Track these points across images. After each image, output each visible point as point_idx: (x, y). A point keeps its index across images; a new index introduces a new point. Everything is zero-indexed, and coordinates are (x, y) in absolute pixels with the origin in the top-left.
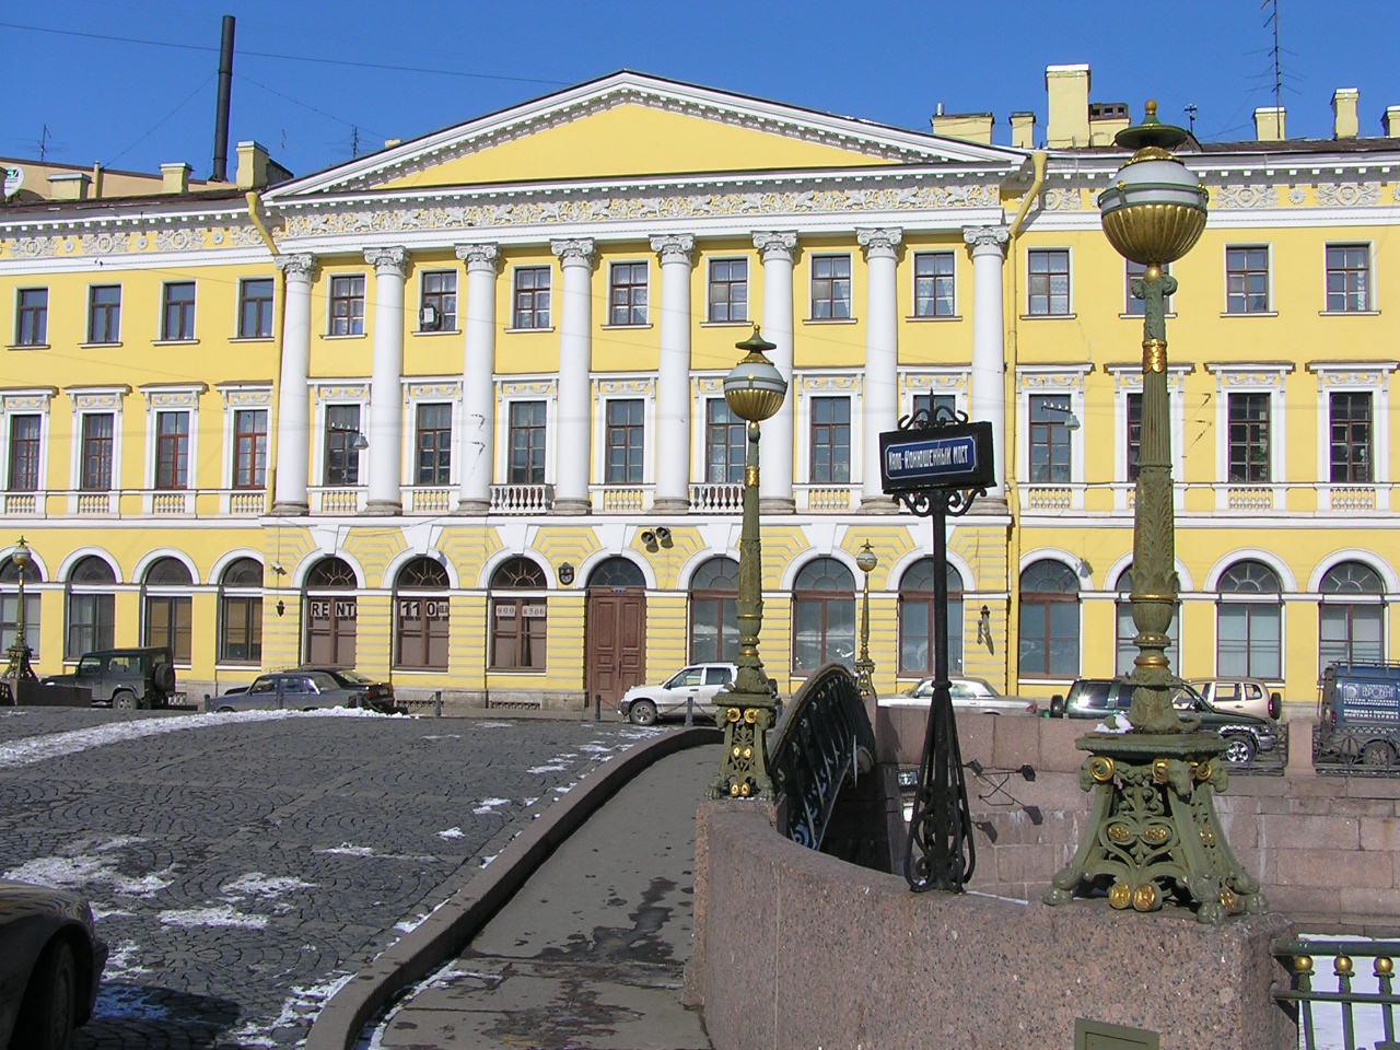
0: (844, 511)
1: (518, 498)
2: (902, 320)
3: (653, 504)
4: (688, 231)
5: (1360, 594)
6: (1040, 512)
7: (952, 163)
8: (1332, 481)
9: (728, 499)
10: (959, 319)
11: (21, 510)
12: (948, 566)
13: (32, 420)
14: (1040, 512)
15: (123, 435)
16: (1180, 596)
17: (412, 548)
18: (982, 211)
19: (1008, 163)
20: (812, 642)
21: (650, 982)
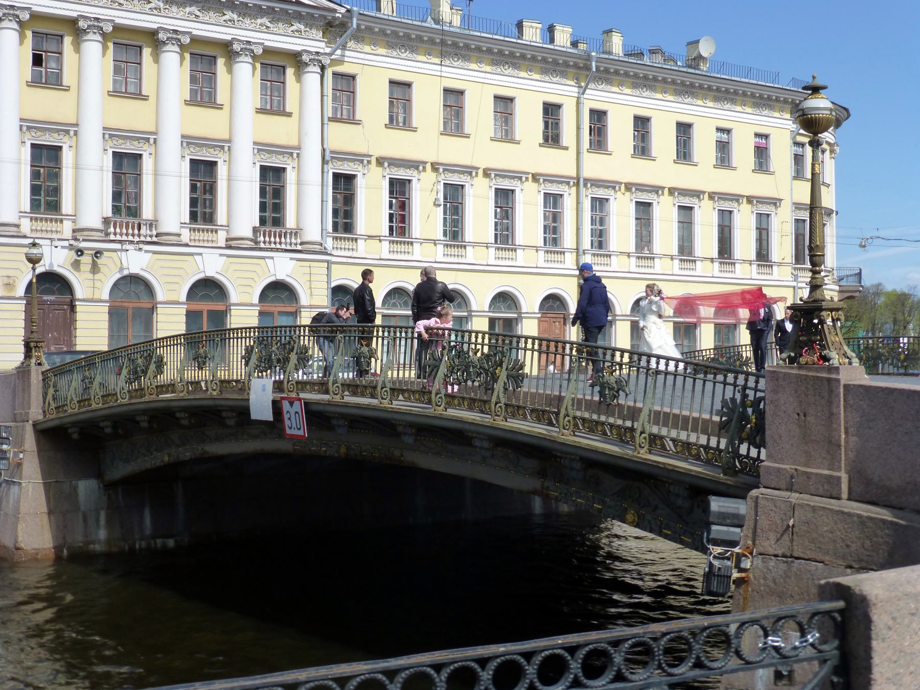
1: (275, 237)
2: (326, 121)
3: (71, 232)
4: (110, 18)
5: (504, 313)
6: (550, 265)
8: (757, 261)
9: (121, 231)
10: (735, 169)
14: (550, 265)
16: (539, 315)
19: (335, 11)
20: (304, 340)
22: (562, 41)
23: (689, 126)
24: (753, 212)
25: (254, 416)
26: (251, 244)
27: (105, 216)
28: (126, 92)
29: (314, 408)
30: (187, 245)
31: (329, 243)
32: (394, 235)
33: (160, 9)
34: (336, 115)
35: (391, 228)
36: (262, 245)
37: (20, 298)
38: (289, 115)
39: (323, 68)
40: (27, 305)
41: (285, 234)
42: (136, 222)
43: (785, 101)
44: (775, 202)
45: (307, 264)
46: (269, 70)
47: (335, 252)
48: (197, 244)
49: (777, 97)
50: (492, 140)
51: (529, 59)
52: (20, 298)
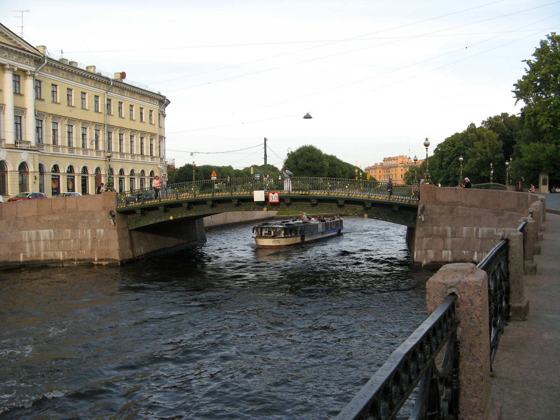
7: (28, 51)
18: (29, 67)
36: (19, 147)
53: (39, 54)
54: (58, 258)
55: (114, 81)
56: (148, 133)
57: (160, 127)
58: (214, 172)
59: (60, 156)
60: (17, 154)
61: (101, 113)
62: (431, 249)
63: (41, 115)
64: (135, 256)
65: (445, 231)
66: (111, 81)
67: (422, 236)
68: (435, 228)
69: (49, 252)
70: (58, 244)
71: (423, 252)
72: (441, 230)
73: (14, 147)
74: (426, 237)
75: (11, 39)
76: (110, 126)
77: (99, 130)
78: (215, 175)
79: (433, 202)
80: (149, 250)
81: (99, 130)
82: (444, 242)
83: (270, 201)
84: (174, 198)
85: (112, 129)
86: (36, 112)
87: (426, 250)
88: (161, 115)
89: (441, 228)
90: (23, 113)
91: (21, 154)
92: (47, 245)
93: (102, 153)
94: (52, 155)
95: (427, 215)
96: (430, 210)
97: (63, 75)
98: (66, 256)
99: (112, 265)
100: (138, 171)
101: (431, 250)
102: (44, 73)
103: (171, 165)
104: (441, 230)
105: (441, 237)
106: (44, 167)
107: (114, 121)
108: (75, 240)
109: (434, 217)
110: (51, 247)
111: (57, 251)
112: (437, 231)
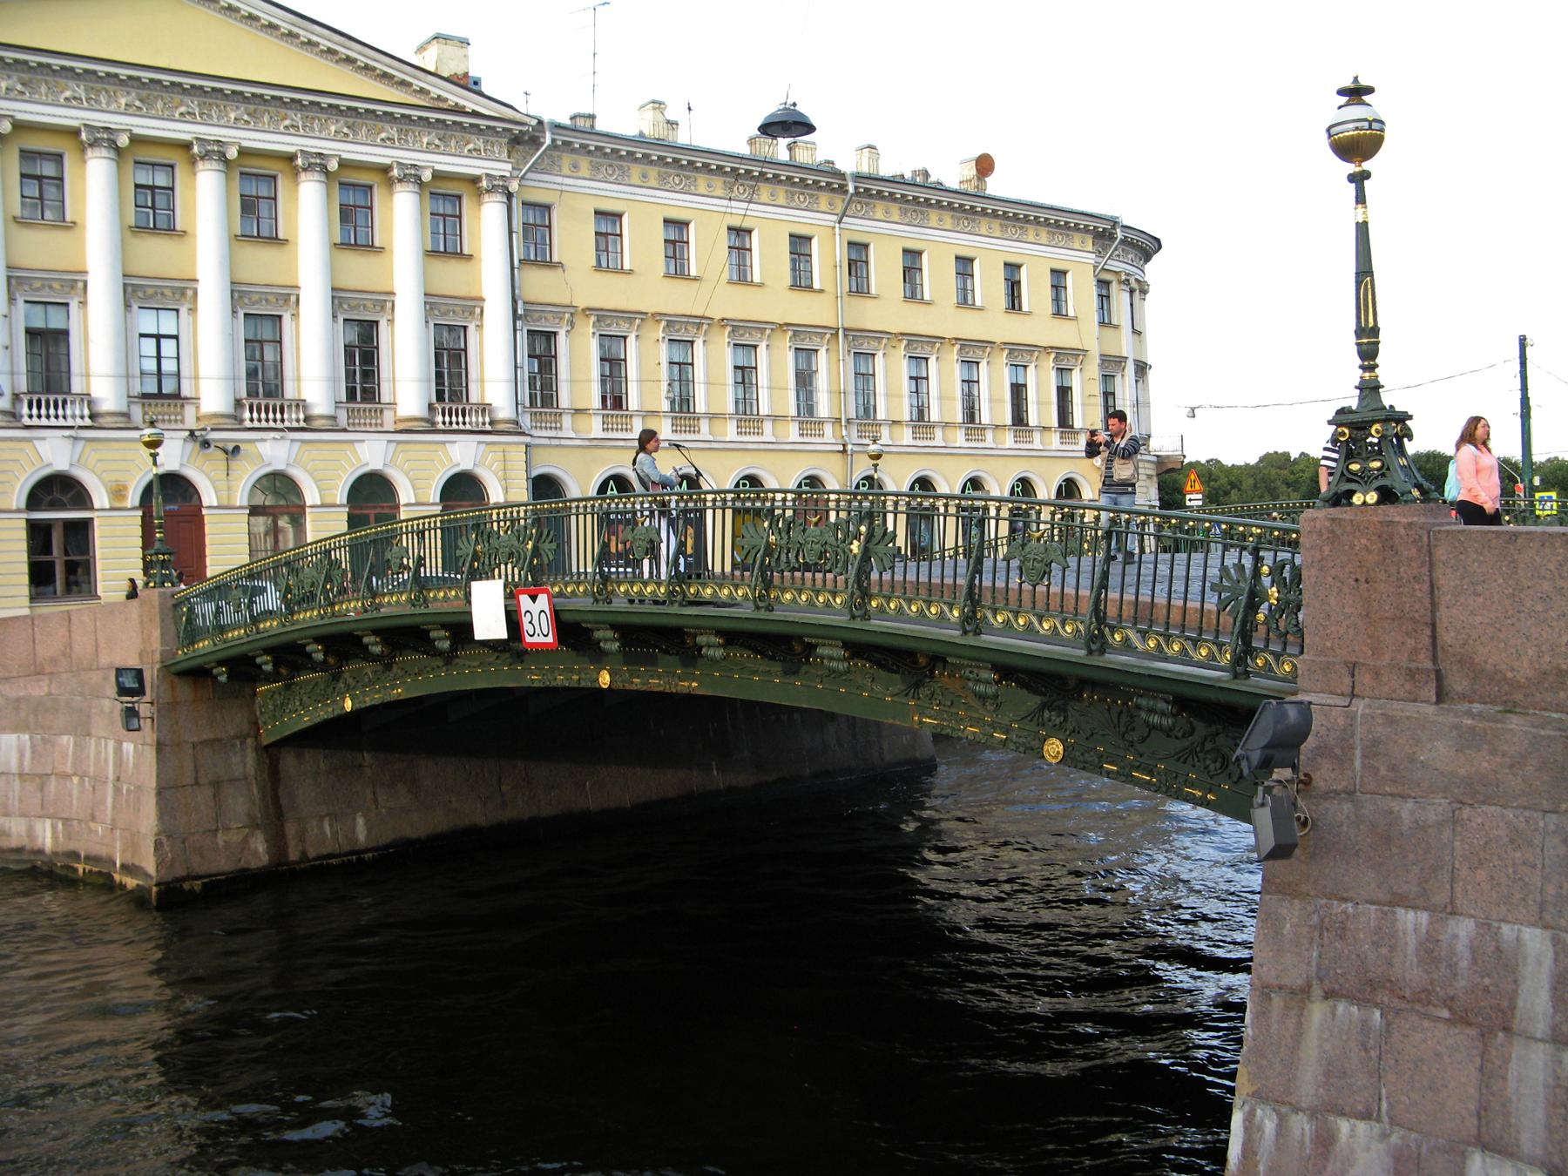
0: (380, 429)
1: (457, 416)
7: (475, 114)
11: (612, 429)
12: (196, 496)
13: (61, 337)
15: (640, 381)
17: (368, 464)
18: (495, 165)
21: (961, 576)
22: (661, 132)
23: (683, 225)
24: (849, 351)
25: (480, 634)
26: (426, 426)
27: (238, 397)
28: (259, 236)
29: (566, 617)
30: (345, 430)
31: (526, 421)
32: (359, 399)
33: (298, 127)
34: (529, 255)
35: (604, 399)
36: (441, 426)
37: (134, 509)
38: (1116, 327)
39: (509, 196)
40: (143, 518)
41: (471, 410)
42: (278, 404)
43: (1086, 230)
44: (1078, 354)
45: (500, 448)
46: (441, 202)
47: (534, 432)
48: (363, 429)
49: (762, 174)
50: (287, 240)
51: (527, 141)
52: (134, 509)
53: (518, 117)
54: (39, 844)
55: (858, 177)
56: (1047, 349)
57: (1137, 332)
58: (1193, 477)
59: (563, 442)
60: (344, 446)
61: (821, 291)
62: (1366, 1116)
63: (549, 316)
64: (294, 855)
65: (1504, 963)
66: (849, 178)
67: (1295, 979)
68: (1411, 921)
69: (13, 819)
70: (42, 790)
71: (1301, 1126)
72: (1462, 947)
73: (425, 426)
74: (1329, 995)
75: (404, 84)
76: (854, 335)
77: (817, 351)
78: (1197, 488)
79: (1412, 674)
80: (387, 836)
81: (817, 351)
82: (1490, 1074)
83: (528, 639)
84: (834, 594)
85: (874, 344)
86: (520, 304)
87: (1324, 1111)
88: (1114, 287)
89: (1463, 929)
90: (472, 313)
91: (356, 445)
92: (11, 794)
93: (828, 429)
94: (595, 443)
95: (1350, 793)
96: (1373, 749)
97: (644, 176)
98: (61, 839)
99: (139, 899)
100: (998, 487)
101: (1362, 1127)
102: (558, 179)
103: (1168, 457)
104: (1462, 947)
105: (1461, 1019)
106: (566, 485)
107: (870, 315)
108: (82, 778)
109: (1406, 810)
110: (21, 801)
111: (36, 817)
112: (1430, 950)
